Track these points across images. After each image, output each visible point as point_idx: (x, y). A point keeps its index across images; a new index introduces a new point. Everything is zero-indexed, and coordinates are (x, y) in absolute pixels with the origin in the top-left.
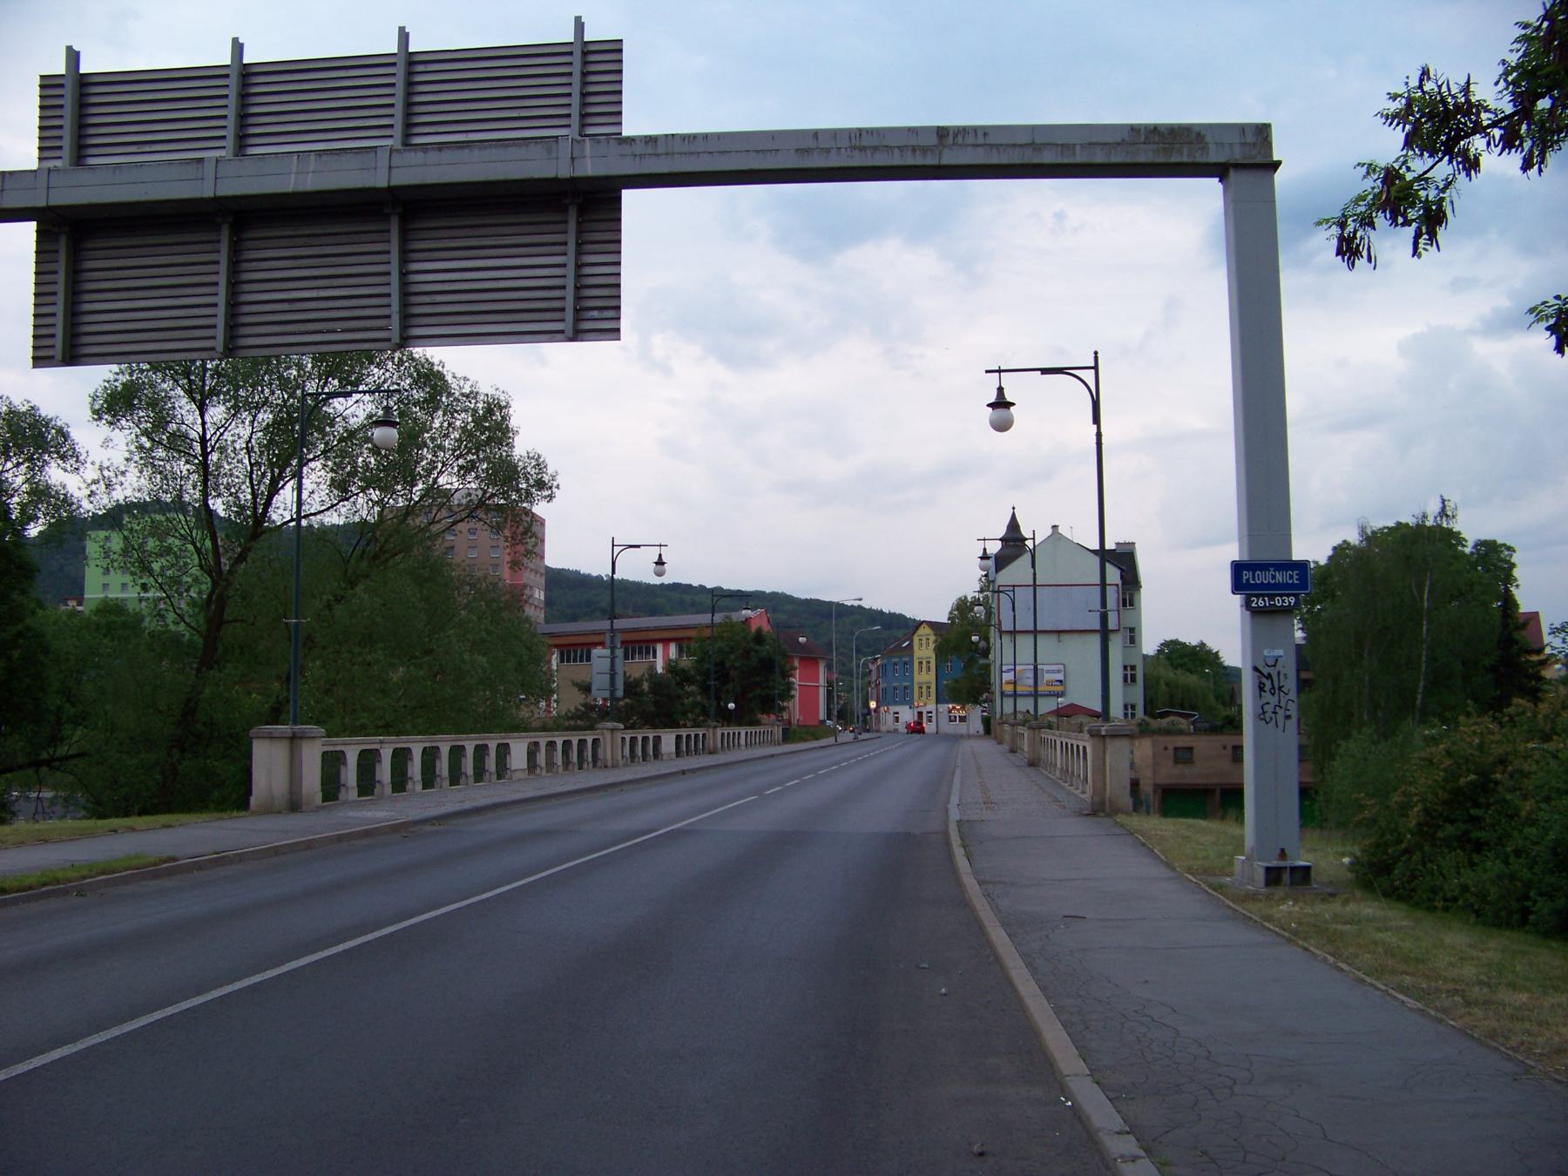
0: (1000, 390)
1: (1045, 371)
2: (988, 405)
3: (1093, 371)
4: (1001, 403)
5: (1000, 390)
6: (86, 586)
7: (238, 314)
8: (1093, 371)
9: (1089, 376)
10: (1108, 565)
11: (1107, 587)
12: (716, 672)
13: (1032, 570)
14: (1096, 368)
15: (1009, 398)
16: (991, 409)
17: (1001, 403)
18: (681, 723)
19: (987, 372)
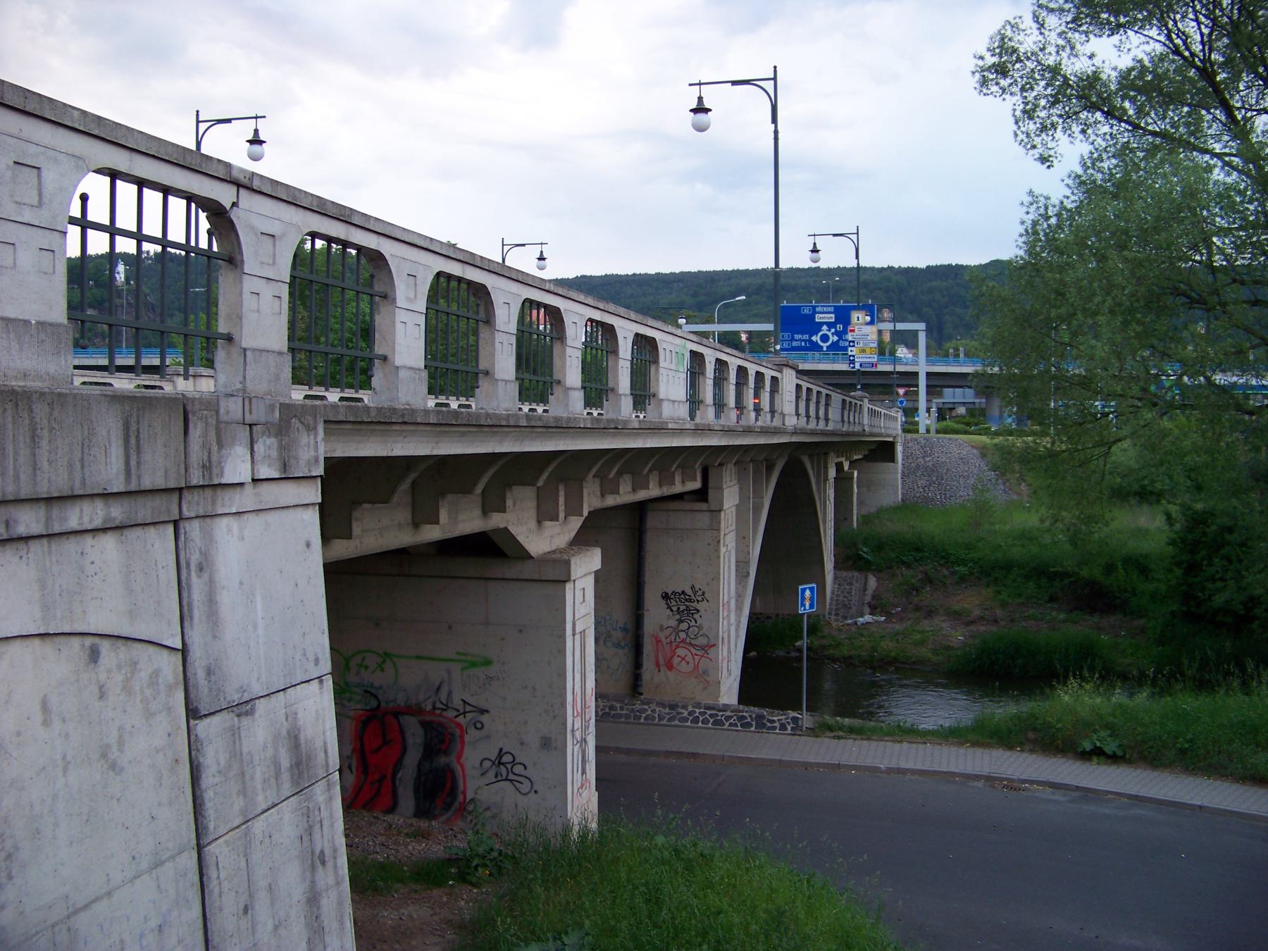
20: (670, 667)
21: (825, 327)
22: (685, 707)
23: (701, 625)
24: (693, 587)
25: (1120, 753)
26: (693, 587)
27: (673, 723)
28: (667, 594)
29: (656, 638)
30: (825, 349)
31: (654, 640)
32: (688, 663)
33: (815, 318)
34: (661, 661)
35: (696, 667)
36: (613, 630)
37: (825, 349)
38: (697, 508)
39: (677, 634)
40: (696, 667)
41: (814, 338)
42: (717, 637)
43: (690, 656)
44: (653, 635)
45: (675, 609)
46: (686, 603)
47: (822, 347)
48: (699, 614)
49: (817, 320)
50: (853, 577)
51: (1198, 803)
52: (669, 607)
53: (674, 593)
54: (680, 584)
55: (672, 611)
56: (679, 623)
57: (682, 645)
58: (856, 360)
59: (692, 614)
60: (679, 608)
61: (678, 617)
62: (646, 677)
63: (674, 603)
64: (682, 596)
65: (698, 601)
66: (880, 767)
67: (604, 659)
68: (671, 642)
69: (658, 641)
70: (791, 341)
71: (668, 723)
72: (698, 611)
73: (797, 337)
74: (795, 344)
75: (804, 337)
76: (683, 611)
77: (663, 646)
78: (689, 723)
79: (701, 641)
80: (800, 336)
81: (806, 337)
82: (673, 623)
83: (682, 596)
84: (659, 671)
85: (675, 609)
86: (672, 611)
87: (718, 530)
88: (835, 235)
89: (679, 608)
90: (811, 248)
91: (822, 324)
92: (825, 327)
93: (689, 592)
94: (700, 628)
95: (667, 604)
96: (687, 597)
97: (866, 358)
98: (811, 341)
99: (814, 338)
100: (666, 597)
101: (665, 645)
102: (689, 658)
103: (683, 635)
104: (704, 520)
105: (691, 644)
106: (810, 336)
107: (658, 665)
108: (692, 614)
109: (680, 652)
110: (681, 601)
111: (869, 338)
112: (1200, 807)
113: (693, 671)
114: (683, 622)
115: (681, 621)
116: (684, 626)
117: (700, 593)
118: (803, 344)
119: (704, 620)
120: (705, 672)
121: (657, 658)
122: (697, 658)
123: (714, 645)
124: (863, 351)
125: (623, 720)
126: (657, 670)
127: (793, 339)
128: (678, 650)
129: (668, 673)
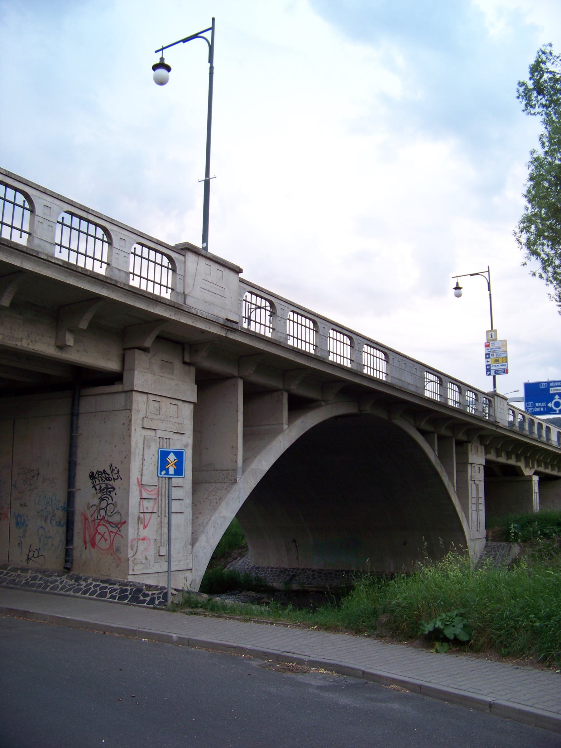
0: (457, 283)
1: (472, 275)
2: (454, 289)
3: (488, 273)
4: (458, 288)
5: (457, 283)
6: (124, 377)
7: (173, 370)
8: (488, 273)
9: (486, 275)
10: (143, 518)
11: (260, 309)
12: (539, 465)
13: (209, 64)
14: (489, 271)
15: (460, 286)
16: (454, 290)
17: (458, 288)
18: (488, 561)
19: (488, 266)
20: (93, 545)
21: (557, 397)
22: (86, 580)
23: (116, 502)
24: (111, 466)
25: (464, 637)
26: (111, 466)
27: (68, 593)
28: (93, 473)
29: (85, 516)
30: (558, 412)
31: (83, 517)
32: (106, 540)
33: (549, 390)
34: (88, 539)
35: (111, 545)
36: (57, 509)
37: (558, 412)
38: (115, 391)
39: (99, 512)
40: (111, 545)
41: (549, 405)
42: (127, 514)
43: (107, 532)
44: (82, 514)
45: (98, 487)
46: (107, 482)
47: (555, 411)
48: (114, 492)
49: (551, 392)
50: (501, 545)
51: (489, 699)
52: (94, 487)
53: (98, 472)
54: (101, 465)
55: (96, 489)
56: (101, 502)
57: (102, 522)
58: (492, 368)
59: (110, 492)
60: (101, 487)
61: (100, 495)
62: (76, 554)
63: (97, 482)
64: (103, 475)
65: (114, 479)
66: (172, 637)
67: (50, 537)
68: (95, 520)
69: (86, 519)
70: (534, 407)
71: (37, 589)
72: (114, 489)
73: (537, 404)
74: (536, 410)
75: (543, 404)
76: (104, 490)
77: (89, 523)
78: (116, 600)
79: (116, 519)
80: (540, 404)
81: (544, 404)
82: (96, 501)
83: (103, 475)
84: (86, 548)
85: (98, 487)
86: (96, 489)
87: (130, 410)
88: (472, 275)
89: (101, 487)
90: (455, 286)
91: (555, 394)
92: (557, 397)
93: (108, 471)
94: (115, 505)
95: (93, 483)
96: (107, 476)
97: (499, 366)
98: (547, 407)
99: (549, 405)
100: (92, 476)
101: (90, 523)
102: (107, 536)
103: (103, 513)
104: (121, 398)
105: (109, 522)
106: (547, 403)
107: (85, 542)
108: (110, 492)
109: (102, 529)
110: (102, 480)
111: (501, 350)
112: (491, 705)
113: (110, 547)
114: (103, 500)
115: (102, 499)
116: (104, 504)
117: (115, 472)
118: (542, 409)
119: (117, 497)
120: (118, 550)
121: (85, 538)
122: (113, 535)
123: (125, 522)
124: (497, 361)
125: (34, 589)
126: (84, 547)
127: (535, 407)
128: (99, 527)
129: (92, 550)
